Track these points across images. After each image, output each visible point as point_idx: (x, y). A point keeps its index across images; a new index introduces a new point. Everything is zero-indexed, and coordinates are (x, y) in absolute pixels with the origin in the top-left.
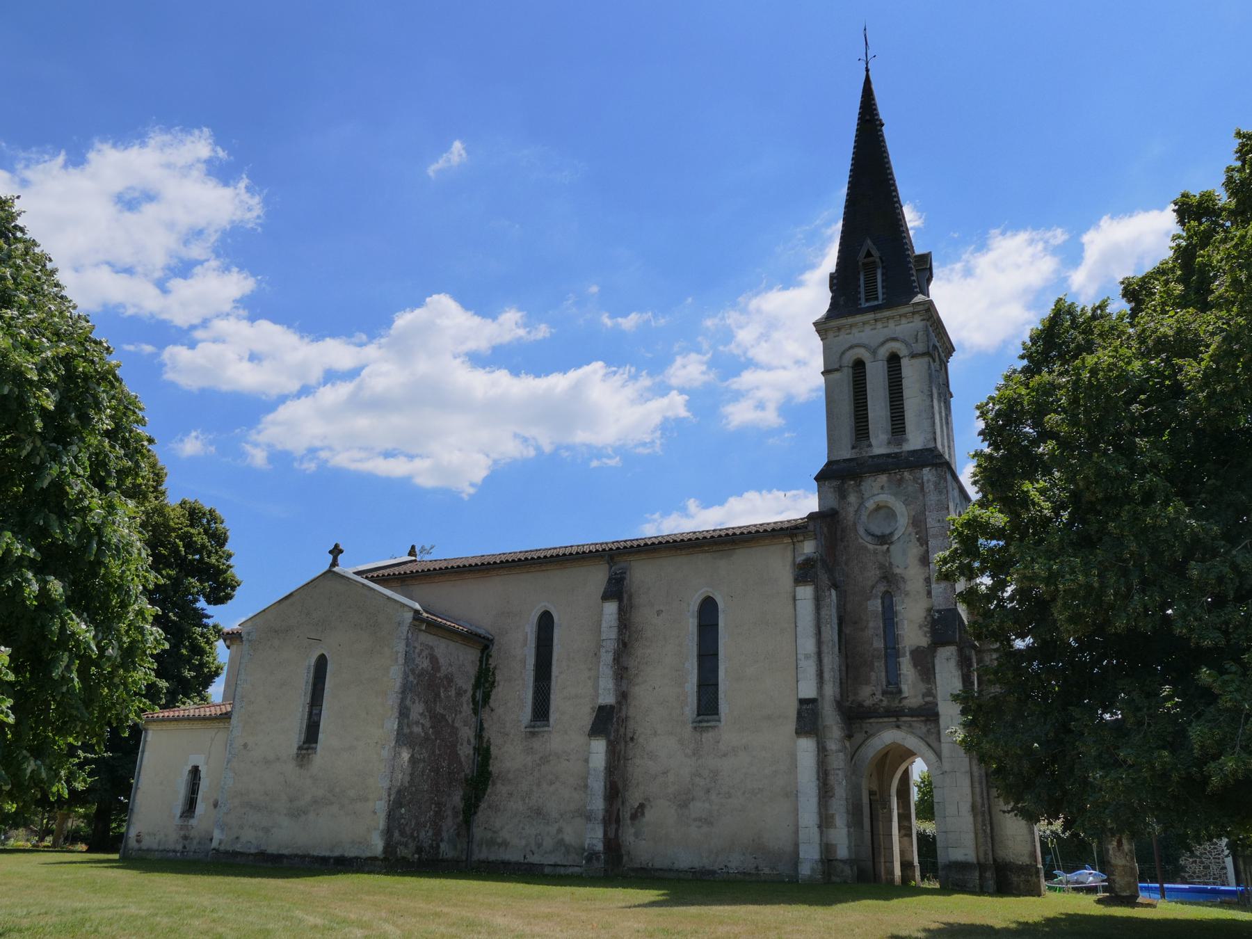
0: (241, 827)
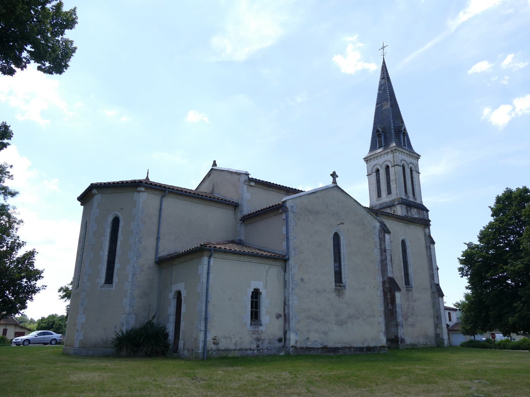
0: (309, 332)
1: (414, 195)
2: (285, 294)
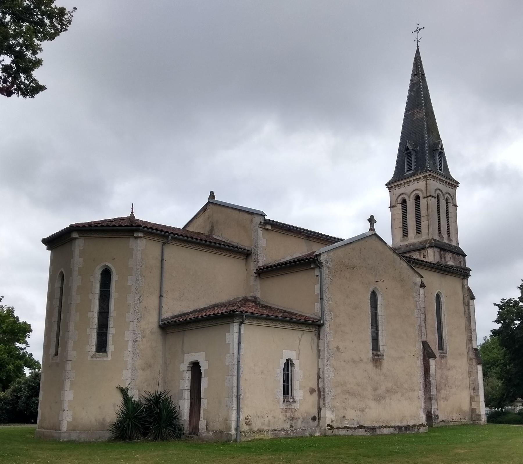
0: (345, 409)
1: (449, 235)
2: (318, 365)
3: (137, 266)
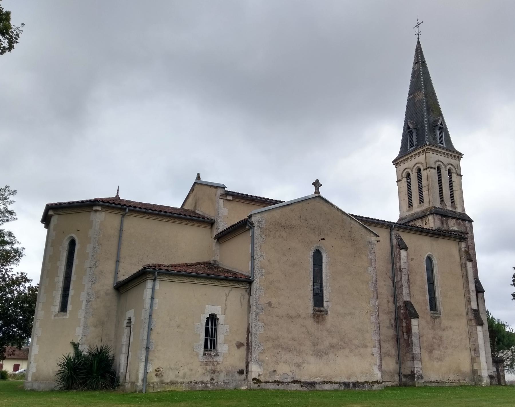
1: (453, 202)
3: (95, 236)
